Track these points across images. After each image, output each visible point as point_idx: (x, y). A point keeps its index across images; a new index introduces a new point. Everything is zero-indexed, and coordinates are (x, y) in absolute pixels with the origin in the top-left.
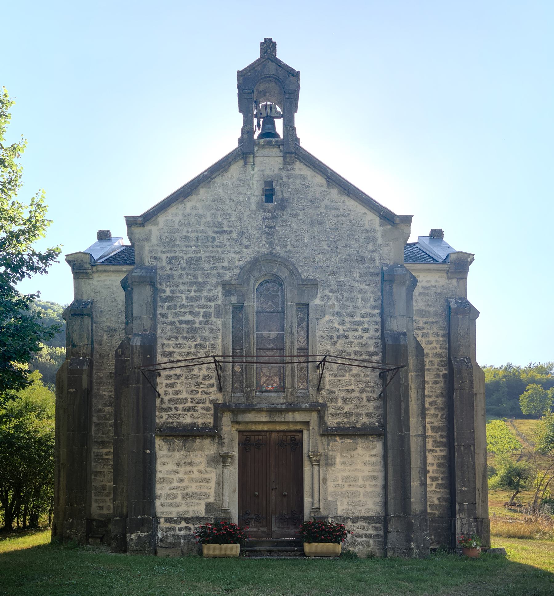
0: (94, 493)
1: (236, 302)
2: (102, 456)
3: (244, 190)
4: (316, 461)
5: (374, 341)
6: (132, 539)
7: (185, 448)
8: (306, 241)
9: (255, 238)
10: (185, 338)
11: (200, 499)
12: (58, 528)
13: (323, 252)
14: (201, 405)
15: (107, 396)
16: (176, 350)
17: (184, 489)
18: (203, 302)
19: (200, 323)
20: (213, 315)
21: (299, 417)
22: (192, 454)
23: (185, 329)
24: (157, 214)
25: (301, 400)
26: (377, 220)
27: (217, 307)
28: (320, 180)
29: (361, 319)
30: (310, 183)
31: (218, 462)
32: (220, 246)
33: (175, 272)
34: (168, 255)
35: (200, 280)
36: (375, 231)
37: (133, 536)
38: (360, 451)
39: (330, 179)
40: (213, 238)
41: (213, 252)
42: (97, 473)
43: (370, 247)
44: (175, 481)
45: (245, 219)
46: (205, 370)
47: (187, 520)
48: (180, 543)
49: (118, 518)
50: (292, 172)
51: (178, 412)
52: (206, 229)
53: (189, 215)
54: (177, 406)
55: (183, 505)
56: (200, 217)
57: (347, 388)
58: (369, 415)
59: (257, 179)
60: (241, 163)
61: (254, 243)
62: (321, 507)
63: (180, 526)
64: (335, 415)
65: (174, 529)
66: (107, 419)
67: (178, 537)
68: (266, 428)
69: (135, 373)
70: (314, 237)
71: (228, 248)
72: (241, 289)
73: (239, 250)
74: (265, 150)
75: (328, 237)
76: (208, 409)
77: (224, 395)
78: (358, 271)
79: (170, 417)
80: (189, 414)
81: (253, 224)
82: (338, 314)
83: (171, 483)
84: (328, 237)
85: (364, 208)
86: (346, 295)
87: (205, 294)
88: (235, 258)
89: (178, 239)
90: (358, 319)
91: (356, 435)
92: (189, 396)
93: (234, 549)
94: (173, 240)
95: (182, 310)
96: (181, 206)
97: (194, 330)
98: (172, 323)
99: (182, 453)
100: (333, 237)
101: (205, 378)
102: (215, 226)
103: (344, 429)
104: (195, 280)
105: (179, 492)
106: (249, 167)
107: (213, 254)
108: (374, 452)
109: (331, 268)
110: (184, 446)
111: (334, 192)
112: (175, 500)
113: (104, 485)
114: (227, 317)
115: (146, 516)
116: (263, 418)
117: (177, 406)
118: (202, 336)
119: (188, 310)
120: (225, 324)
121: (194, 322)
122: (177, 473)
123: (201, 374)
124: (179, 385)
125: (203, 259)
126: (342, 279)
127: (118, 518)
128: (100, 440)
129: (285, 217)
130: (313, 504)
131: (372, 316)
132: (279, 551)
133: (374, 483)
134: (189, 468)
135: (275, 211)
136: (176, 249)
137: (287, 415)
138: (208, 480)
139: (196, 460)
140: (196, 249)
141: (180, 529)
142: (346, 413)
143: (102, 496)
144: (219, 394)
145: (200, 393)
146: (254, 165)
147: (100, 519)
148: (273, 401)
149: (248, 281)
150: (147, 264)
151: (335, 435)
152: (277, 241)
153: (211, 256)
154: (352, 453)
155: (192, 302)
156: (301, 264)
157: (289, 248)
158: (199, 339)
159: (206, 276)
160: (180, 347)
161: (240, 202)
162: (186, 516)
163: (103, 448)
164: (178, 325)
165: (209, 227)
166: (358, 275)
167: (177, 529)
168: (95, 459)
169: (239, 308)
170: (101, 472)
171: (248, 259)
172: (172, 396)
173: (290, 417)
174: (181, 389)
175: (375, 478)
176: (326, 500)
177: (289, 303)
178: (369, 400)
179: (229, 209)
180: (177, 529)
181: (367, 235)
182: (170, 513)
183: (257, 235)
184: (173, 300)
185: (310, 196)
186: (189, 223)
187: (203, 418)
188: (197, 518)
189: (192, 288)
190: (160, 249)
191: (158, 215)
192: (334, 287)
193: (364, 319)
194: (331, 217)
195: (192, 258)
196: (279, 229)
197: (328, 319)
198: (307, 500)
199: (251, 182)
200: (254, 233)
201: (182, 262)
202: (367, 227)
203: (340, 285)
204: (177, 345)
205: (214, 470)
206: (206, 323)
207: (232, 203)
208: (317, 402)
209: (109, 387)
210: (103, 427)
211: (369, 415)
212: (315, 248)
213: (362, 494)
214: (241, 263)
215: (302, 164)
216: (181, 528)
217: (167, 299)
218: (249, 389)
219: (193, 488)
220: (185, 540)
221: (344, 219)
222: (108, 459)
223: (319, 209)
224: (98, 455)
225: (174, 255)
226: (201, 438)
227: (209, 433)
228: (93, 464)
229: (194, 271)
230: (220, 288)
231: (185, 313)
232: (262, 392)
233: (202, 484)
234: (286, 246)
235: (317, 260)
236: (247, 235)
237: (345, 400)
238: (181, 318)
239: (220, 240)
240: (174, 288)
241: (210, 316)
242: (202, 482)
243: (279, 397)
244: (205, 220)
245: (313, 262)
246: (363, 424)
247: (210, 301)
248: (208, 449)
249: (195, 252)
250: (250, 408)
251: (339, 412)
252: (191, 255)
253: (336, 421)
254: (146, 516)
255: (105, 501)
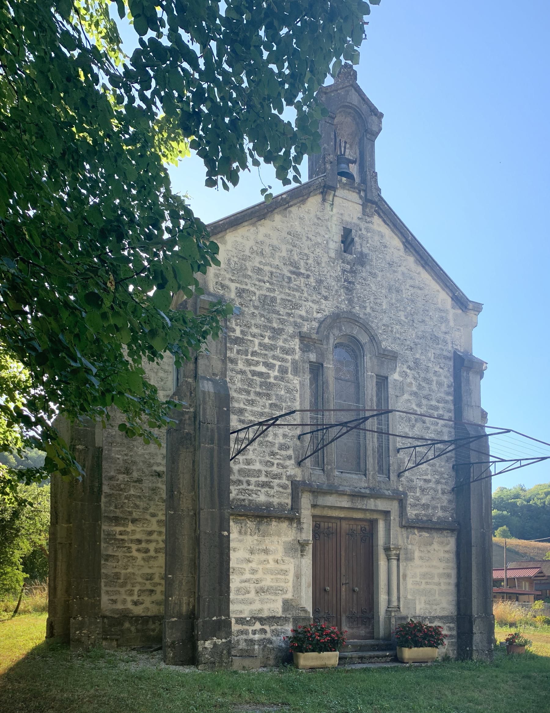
0: (105, 582)
1: (314, 360)
2: (115, 535)
3: (322, 231)
4: (395, 554)
5: (448, 429)
6: (205, 648)
7: (259, 531)
8: (384, 307)
9: (334, 290)
10: (258, 394)
11: (276, 594)
12: (55, 627)
13: (399, 322)
14: (277, 481)
15: (121, 459)
16: (248, 408)
17: (257, 581)
18: (278, 352)
19: (276, 378)
20: (290, 371)
21: (381, 505)
22: (267, 540)
23: (258, 383)
24: (226, 230)
25: (383, 486)
26: (449, 301)
27: (294, 363)
28: (395, 242)
29: (437, 404)
30: (388, 243)
31: (296, 550)
32: (297, 290)
33: (246, 309)
34: (238, 285)
35: (275, 325)
36: (446, 311)
37: (208, 644)
38: (436, 546)
39: (409, 243)
40: (290, 278)
41: (289, 295)
42: (108, 557)
43: (443, 328)
44: (247, 571)
45: (323, 265)
46: (281, 438)
47: (261, 620)
48: (254, 649)
49: (175, 619)
50: (370, 225)
51: (250, 487)
52: (281, 265)
53: (262, 243)
54: (250, 479)
55: (257, 602)
56: (274, 249)
57: (425, 477)
58: (444, 509)
59: (336, 222)
60: (319, 198)
61: (333, 296)
62: (401, 606)
63: (254, 628)
64: (414, 506)
65: (246, 632)
66: (121, 490)
67: (251, 642)
68: (342, 514)
69: (207, 429)
70: (392, 305)
71: (306, 295)
72: (321, 346)
73: (317, 300)
74: (345, 191)
75: (405, 308)
76: (284, 487)
77: (303, 471)
78: (433, 351)
79: (240, 492)
80: (263, 490)
81: (332, 273)
82: (415, 394)
83: (242, 574)
84: (405, 308)
85: (437, 285)
86: (422, 375)
87: (280, 343)
88: (315, 309)
89: (249, 268)
90: (434, 403)
91: (434, 529)
92: (264, 468)
93: (331, 658)
94: (243, 269)
95: (255, 358)
96: (253, 229)
97: (270, 386)
98: (242, 372)
99: (256, 537)
100: (409, 308)
101: (283, 447)
102: (291, 264)
103: (421, 521)
104: (270, 325)
105: (252, 586)
106: (327, 205)
107: (289, 298)
108: (447, 548)
109: (408, 342)
110: (258, 529)
111: (411, 260)
112: (247, 596)
113: (117, 573)
114: (306, 376)
115: (223, 618)
116: (345, 502)
117: (250, 479)
118: (278, 395)
119: (261, 360)
120: (303, 385)
121: (268, 376)
122: (249, 561)
123: (276, 442)
124: (251, 452)
125: (278, 301)
126: (418, 356)
127: (175, 619)
128: (112, 515)
129: (364, 274)
130: (389, 601)
131: (446, 402)
132: (371, 657)
133: (447, 581)
134: (263, 557)
135: (354, 264)
136: (246, 280)
137: (369, 501)
138: (285, 572)
139: (272, 548)
140: (270, 287)
141: (254, 632)
142: (424, 505)
143: (115, 586)
144: (297, 469)
145: (275, 465)
146: (333, 204)
147: (112, 615)
148: (355, 484)
149: (328, 337)
150: (211, 290)
151: (414, 527)
152: (356, 299)
153: (287, 300)
154: (429, 548)
155: (266, 350)
156: (380, 332)
157: (368, 310)
158: (274, 397)
159: (282, 322)
160: (252, 404)
161: (318, 244)
162: (260, 615)
163: (116, 526)
164: (250, 376)
165: (284, 264)
166: (433, 355)
167: (250, 632)
168: (105, 539)
169: (317, 370)
170: (114, 556)
171: (327, 313)
172: (242, 466)
173: (372, 504)
174: (253, 457)
175: (449, 576)
176: (406, 598)
177: (369, 373)
178: (443, 493)
179: (307, 249)
180: (250, 632)
181: (440, 314)
182: (241, 612)
183: (336, 287)
184: (243, 343)
185: (388, 258)
186: (262, 253)
187: (279, 497)
188: (274, 617)
189: (266, 334)
190: (228, 276)
191: (228, 231)
192: (411, 364)
193: (440, 405)
194: (407, 287)
195: (266, 296)
196: (358, 287)
197: (407, 398)
198: (383, 598)
199: (329, 224)
200: (333, 284)
201: (254, 298)
202: (440, 306)
203: (417, 362)
204: (249, 400)
205: (292, 560)
206: (282, 379)
207: (309, 242)
208: (398, 489)
209: (124, 449)
210: (116, 499)
211: (444, 509)
212: (393, 317)
213: (437, 592)
214: (319, 315)
215: (380, 220)
216: (255, 630)
217: (237, 341)
218: (329, 467)
219: (268, 581)
220: (260, 645)
221: (419, 292)
222: (123, 540)
223: (396, 274)
224: (109, 535)
225: (244, 287)
226: (277, 520)
227: (289, 516)
228: (103, 545)
229: (269, 313)
230: (297, 340)
231: (258, 363)
232: (342, 472)
233: (279, 576)
234: (365, 308)
235: (395, 330)
236: (325, 284)
237: (423, 490)
238: (253, 368)
239: (297, 283)
240: (245, 329)
241: (286, 372)
242: (279, 574)
243: (361, 480)
244: (281, 255)
245: (392, 331)
246: (439, 518)
247: (287, 354)
248: (285, 535)
249: (269, 290)
250: (332, 490)
251: (417, 502)
252: (264, 292)
253: (415, 512)
254: (223, 618)
255: (119, 593)
